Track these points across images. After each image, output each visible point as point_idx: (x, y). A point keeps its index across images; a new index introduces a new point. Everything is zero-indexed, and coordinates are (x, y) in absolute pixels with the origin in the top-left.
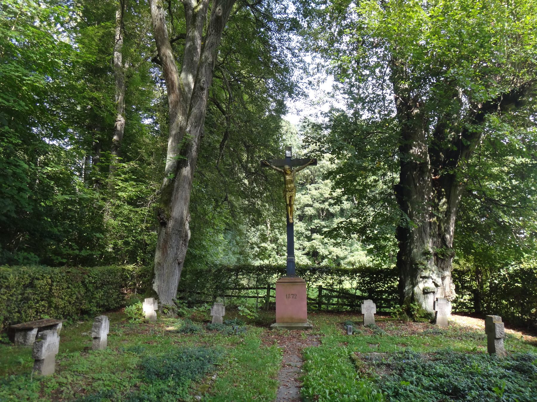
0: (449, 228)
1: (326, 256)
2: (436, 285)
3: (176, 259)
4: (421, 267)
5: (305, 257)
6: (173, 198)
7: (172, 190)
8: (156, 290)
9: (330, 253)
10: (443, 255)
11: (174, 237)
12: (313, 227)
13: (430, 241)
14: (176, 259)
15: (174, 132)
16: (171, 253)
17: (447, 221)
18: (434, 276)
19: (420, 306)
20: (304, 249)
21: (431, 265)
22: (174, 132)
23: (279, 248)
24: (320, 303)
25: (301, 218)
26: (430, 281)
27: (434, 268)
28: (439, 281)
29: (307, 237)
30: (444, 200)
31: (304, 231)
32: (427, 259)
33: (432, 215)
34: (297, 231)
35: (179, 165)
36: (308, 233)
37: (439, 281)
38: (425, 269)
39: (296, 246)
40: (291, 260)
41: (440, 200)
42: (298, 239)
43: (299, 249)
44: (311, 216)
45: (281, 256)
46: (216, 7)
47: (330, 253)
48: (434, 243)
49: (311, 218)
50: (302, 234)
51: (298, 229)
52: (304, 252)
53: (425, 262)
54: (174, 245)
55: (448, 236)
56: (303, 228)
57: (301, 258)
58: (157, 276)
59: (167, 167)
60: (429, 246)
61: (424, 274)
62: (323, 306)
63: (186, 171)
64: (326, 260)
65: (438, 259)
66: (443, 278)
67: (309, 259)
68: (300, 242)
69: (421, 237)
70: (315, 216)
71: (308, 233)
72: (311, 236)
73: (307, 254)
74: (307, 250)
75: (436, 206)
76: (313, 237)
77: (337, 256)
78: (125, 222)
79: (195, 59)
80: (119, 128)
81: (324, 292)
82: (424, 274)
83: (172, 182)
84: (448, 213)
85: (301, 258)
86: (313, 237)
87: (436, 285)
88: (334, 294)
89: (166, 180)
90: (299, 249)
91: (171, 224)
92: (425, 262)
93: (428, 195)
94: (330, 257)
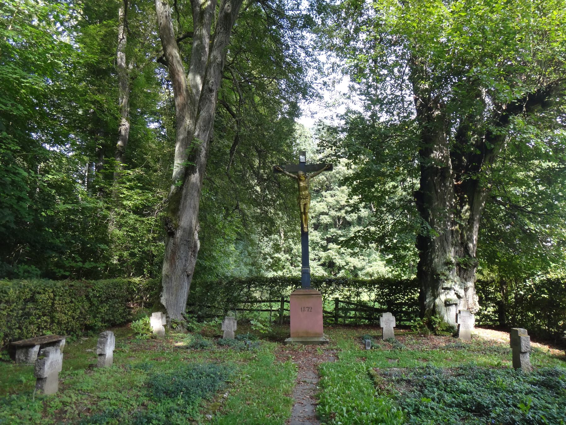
0: (472, 236)
1: (343, 267)
2: (459, 297)
3: (185, 271)
4: (442, 277)
5: (320, 268)
6: (181, 207)
7: (180, 198)
10: (466, 265)
11: (182, 248)
12: (329, 236)
14: (185, 271)
15: (181, 137)
16: (179, 265)
17: (470, 230)
18: (457, 288)
19: (442, 318)
20: (319, 260)
21: (453, 275)
22: (181, 137)
23: (294, 259)
24: (336, 316)
25: (316, 227)
27: (457, 279)
28: (462, 292)
29: (322, 246)
30: (467, 207)
31: (319, 240)
32: (449, 269)
34: (312, 241)
35: (187, 172)
36: (324, 243)
37: (462, 292)
38: (447, 280)
41: (462, 207)
42: (314, 249)
43: (315, 259)
44: (327, 224)
45: (295, 267)
47: (347, 264)
50: (318, 243)
52: (319, 263)
53: (447, 273)
55: (471, 245)
56: (318, 237)
57: (316, 269)
60: (451, 255)
62: (340, 319)
63: (195, 178)
64: (343, 271)
65: (460, 269)
66: (466, 289)
67: (325, 270)
68: (316, 252)
69: (442, 246)
70: (331, 224)
71: (324, 243)
72: (327, 246)
73: (323, 265)
74: (323, 261)
75: (458, 213)
76: (329, 247)
77: (354, 267)
79: (203, 59)
80: (123, 132)
83: (180, 189)
84: (471, 221)
85: (316, 269)
86: (329, 247)
87: (459, 297)
88: (352, 306)
89: (173, 187)
90: (315, 259)
92: (447, 273)
94: (347, 267)
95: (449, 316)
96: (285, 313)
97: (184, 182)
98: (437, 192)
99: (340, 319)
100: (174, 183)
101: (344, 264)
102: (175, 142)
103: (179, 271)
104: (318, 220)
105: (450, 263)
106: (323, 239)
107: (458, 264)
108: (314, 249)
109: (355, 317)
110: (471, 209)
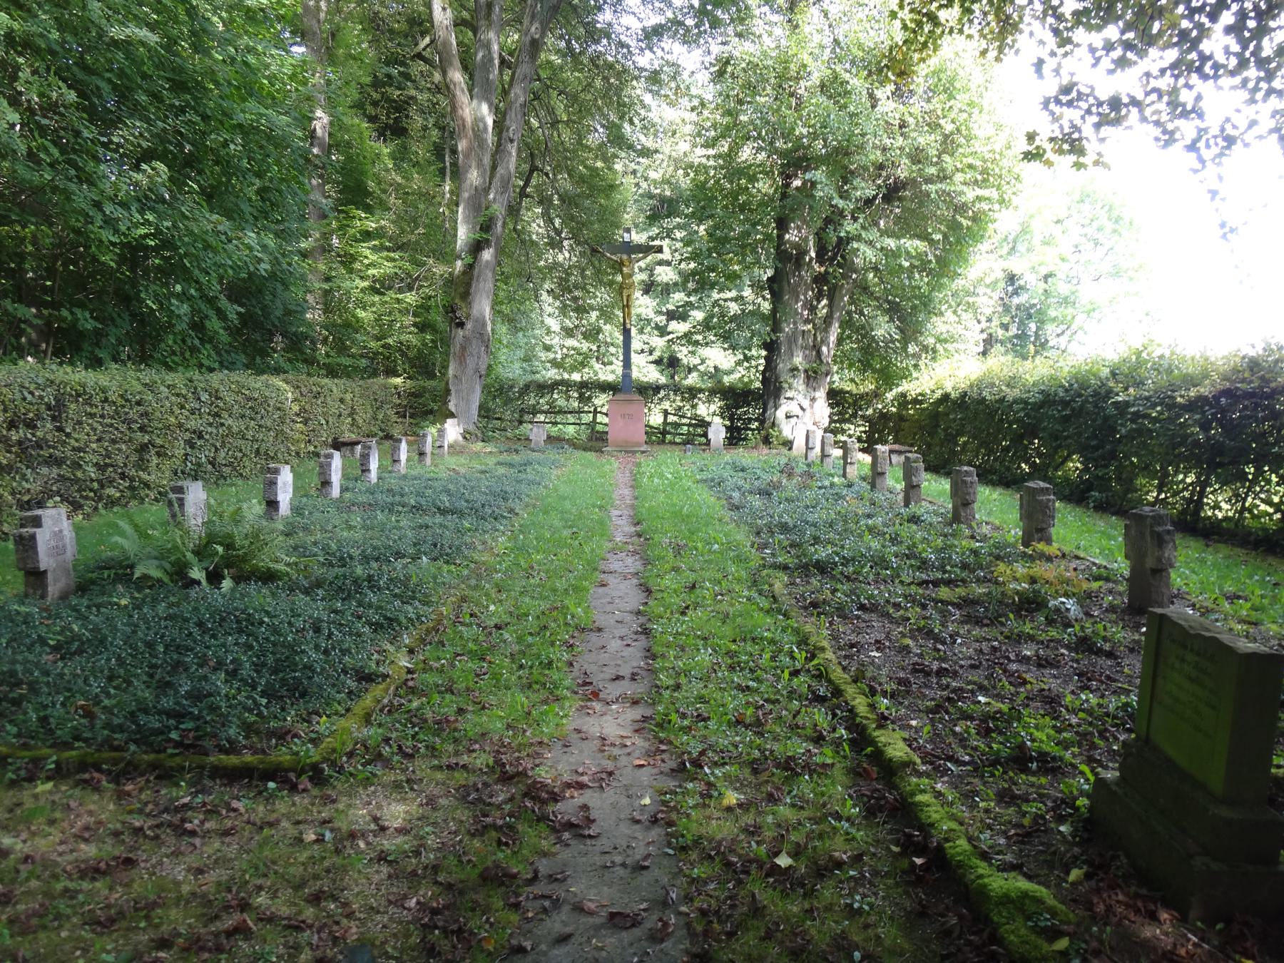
0: (827, 337)
1: (695, 366)
2: (802, 408)
3: (477, 371)
4: (785, 386)
5: (653, 367)
6: (472, 290)
7: (471, 279)
8: (453, 410)
9: (703, 362)
10: (815, 372)
11: (474, 341)
12: (671, 307)
13: (801, 354)
14: (477, 371)
15: (466, 195)
16: (471, 362)
17: (826, 330)
18: (800, 398)
19: (780, 432)
20: (651, 353)
21: (799, 383)
22: (466, 195)
23: (603, 349)
24: (664, 433)
25: (648, 288)
26: (795, 402)
27: (802, 387)
28: (806, 404)
29: (657, 327)
30: (824, 302)
31: (652, 315)
32: (794, 376)
33: (807, 321)
34: (638, 316)
35: (477, 247)
36: (662, 319)
37: (806, 404)
38: (790, 388)
39: (636, 344)
40: (627, 375)
41: (819, 302)
42: (641, 331)
43: (642, 351)
44: (667, 284)
45: (603, 363)
46: (531, 23)
47: (703, 362)
48: (805, 357)
49: (667, 290)
50: (649, 321)
51: (639, 311)
52: (651, 358)
53: (791, 381)
54: (474, 353)
55: (824, 349)
56: (650, 310)
57: (645, 371)
58: (453, 392)
59: (459, 242)
60: (798, 360)
61: (789, 394)
62: (668, 437)
63: (487, 255)
64: (695, 374)
65: (808, 377)
66: (813, 400)
67: (662, 372)
68: (645, 337)
69: (790, 348)
70: (676, 284)
71: (662, 319)
72: (666, 326)
73: (658, 362)
74: (657, 355)
75: (813, 309)
76: (669, 329)
77: (716, 368)
78: (1042, 490)
79: (491, 77)
80: (319, 132)
81: (671, 419)
82: (789, 394)
83: (470, 267)
84: (828, 320)
85: (645, 371)
86: (669, 329)
87: (802, 408)
88: (684, 421)
89: (459, 263)
90: (642, 351)
91: (469, 326)
92: (791, 381)
93: (805, 295)
94: (702, 368)
95: (787, 430)
96: (599, 428)
97: (475, 258)
98: (789, 282)
99: (668, 437)
100: (459, 257)
101: (698, 361)
102: (457, 205)
103: (470, 371)
104: (652, 275)
105: (796, 369)
106: (659, 313)
107: (806, 371)
108: (641, 331)
109: (689, 433)
110: (830, 306)
